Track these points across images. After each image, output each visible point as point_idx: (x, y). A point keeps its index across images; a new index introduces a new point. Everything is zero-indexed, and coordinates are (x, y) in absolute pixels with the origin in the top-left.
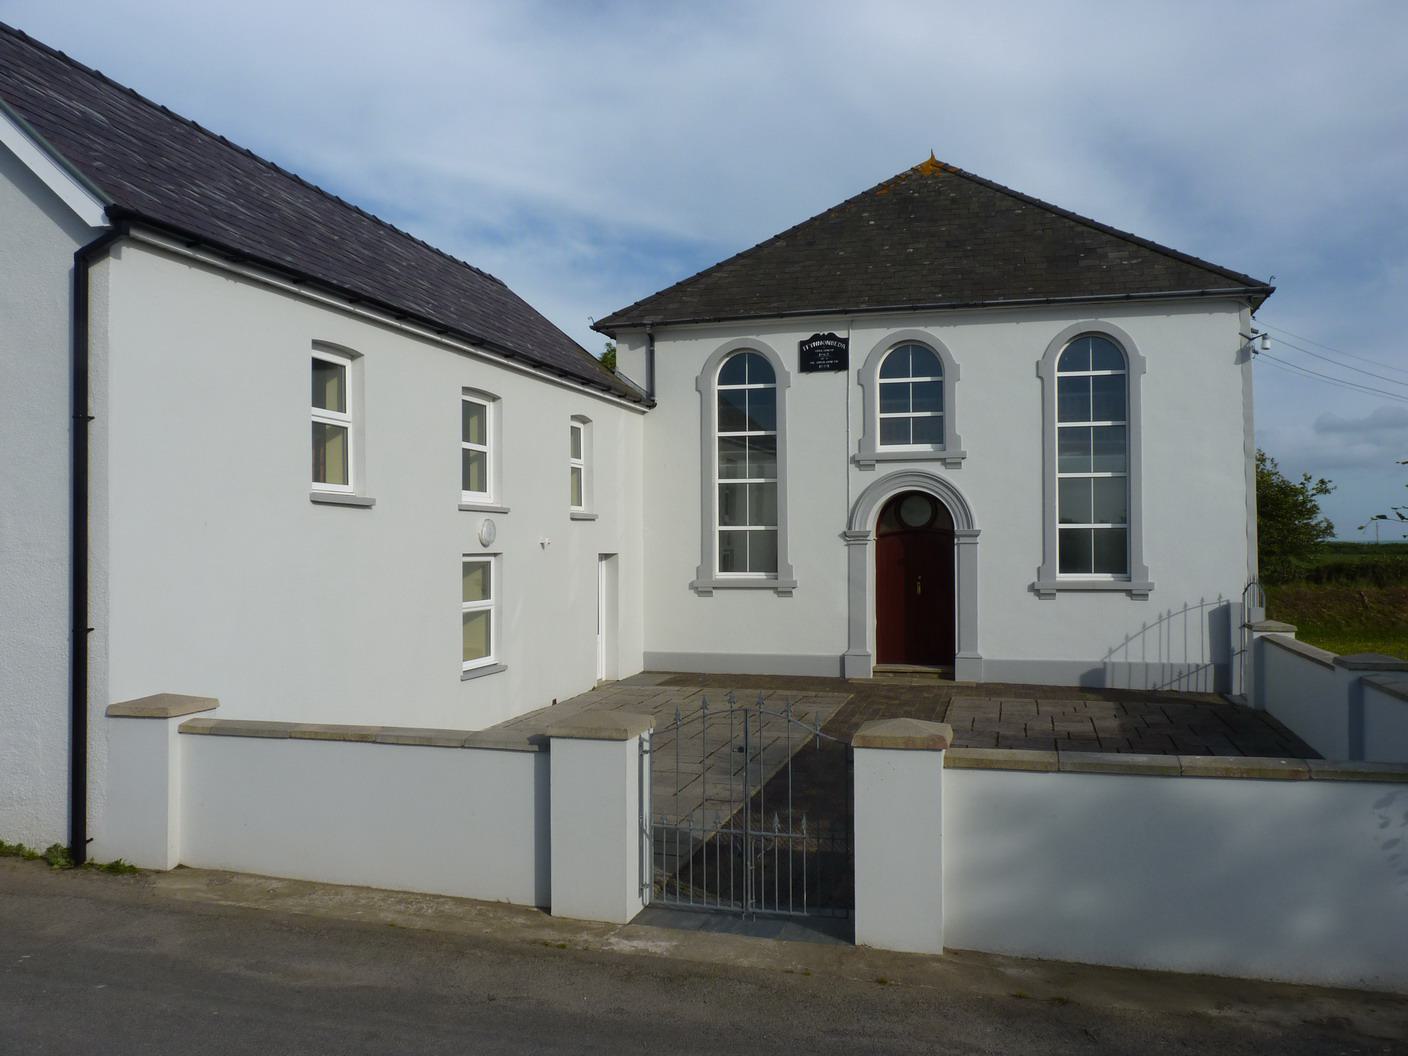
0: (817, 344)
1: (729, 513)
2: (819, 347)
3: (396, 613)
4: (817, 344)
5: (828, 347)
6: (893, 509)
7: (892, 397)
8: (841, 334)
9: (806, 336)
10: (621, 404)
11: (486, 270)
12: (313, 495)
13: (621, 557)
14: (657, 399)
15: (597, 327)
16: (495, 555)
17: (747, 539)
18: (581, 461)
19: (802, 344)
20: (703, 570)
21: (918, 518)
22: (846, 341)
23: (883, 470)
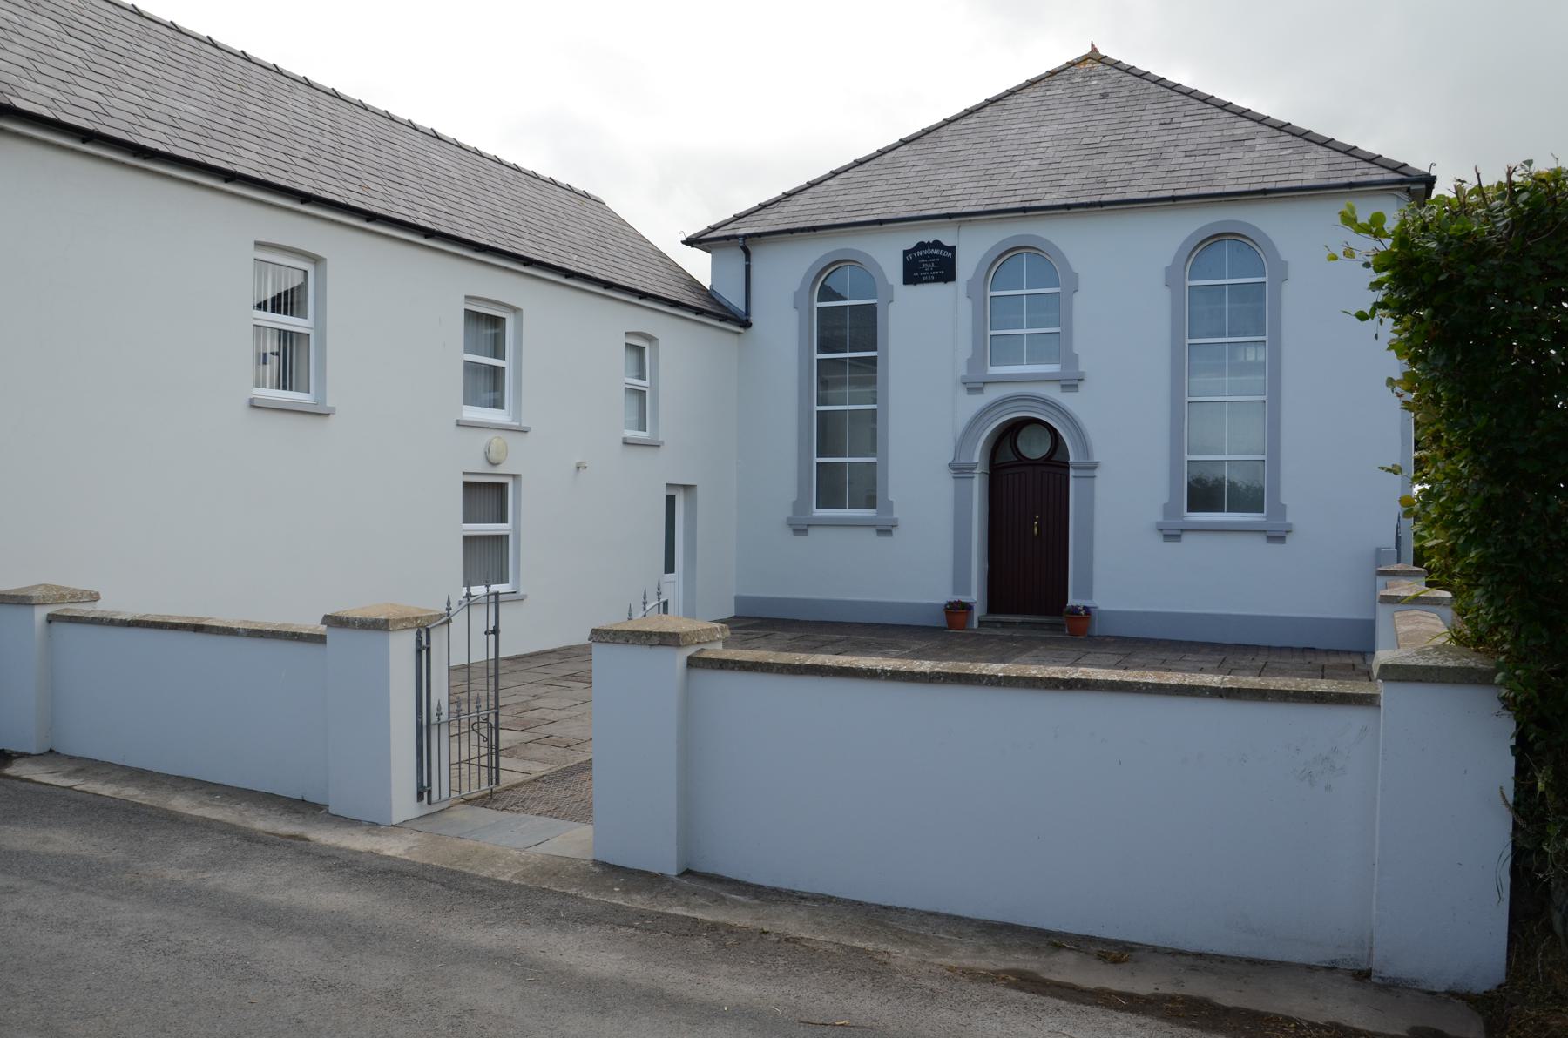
0: (920, 253)
1: (827, 444)
2: (925, 257)
3: (204, 488)
4: (920, 253)
5: (933, 256)
6: (1011, 432)
7: (1004, 311)
8: (947, 242)
9: (911, 245)
10: (429, 247)
11: (526, 165)
12: (252, 400)
13: (699, 490)
14: (753, 319)
15: (689, 242)
16: (514, 476)
17: (842, 470)
18: (646, 383)
19: (906, 253)
20: (800, 506)
21: (1034, 448)
22: (952, 249)
23: (992, 394)
